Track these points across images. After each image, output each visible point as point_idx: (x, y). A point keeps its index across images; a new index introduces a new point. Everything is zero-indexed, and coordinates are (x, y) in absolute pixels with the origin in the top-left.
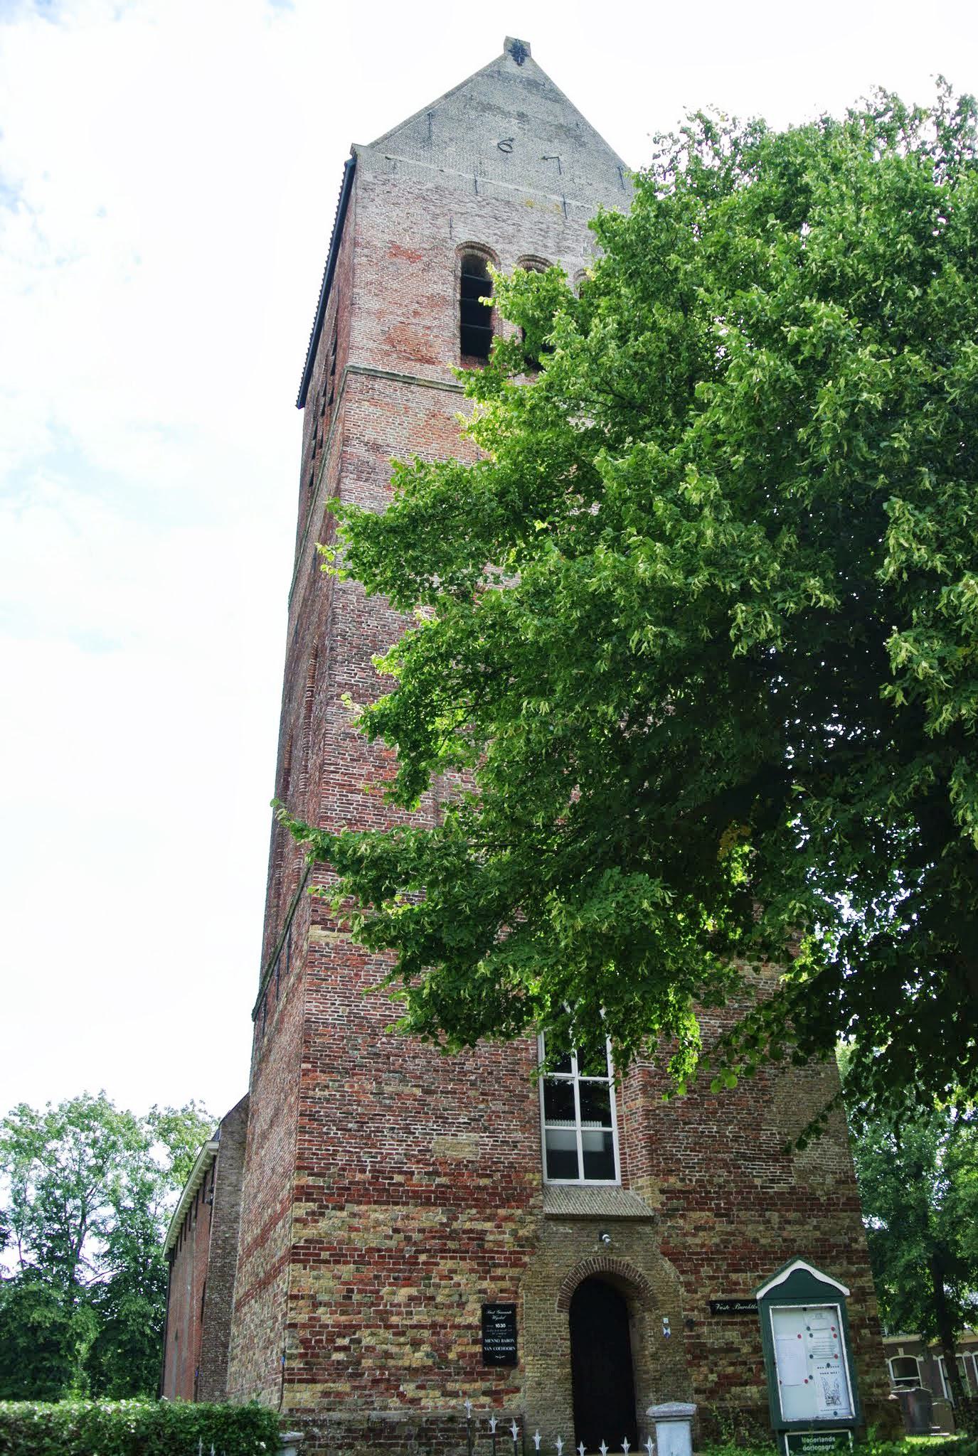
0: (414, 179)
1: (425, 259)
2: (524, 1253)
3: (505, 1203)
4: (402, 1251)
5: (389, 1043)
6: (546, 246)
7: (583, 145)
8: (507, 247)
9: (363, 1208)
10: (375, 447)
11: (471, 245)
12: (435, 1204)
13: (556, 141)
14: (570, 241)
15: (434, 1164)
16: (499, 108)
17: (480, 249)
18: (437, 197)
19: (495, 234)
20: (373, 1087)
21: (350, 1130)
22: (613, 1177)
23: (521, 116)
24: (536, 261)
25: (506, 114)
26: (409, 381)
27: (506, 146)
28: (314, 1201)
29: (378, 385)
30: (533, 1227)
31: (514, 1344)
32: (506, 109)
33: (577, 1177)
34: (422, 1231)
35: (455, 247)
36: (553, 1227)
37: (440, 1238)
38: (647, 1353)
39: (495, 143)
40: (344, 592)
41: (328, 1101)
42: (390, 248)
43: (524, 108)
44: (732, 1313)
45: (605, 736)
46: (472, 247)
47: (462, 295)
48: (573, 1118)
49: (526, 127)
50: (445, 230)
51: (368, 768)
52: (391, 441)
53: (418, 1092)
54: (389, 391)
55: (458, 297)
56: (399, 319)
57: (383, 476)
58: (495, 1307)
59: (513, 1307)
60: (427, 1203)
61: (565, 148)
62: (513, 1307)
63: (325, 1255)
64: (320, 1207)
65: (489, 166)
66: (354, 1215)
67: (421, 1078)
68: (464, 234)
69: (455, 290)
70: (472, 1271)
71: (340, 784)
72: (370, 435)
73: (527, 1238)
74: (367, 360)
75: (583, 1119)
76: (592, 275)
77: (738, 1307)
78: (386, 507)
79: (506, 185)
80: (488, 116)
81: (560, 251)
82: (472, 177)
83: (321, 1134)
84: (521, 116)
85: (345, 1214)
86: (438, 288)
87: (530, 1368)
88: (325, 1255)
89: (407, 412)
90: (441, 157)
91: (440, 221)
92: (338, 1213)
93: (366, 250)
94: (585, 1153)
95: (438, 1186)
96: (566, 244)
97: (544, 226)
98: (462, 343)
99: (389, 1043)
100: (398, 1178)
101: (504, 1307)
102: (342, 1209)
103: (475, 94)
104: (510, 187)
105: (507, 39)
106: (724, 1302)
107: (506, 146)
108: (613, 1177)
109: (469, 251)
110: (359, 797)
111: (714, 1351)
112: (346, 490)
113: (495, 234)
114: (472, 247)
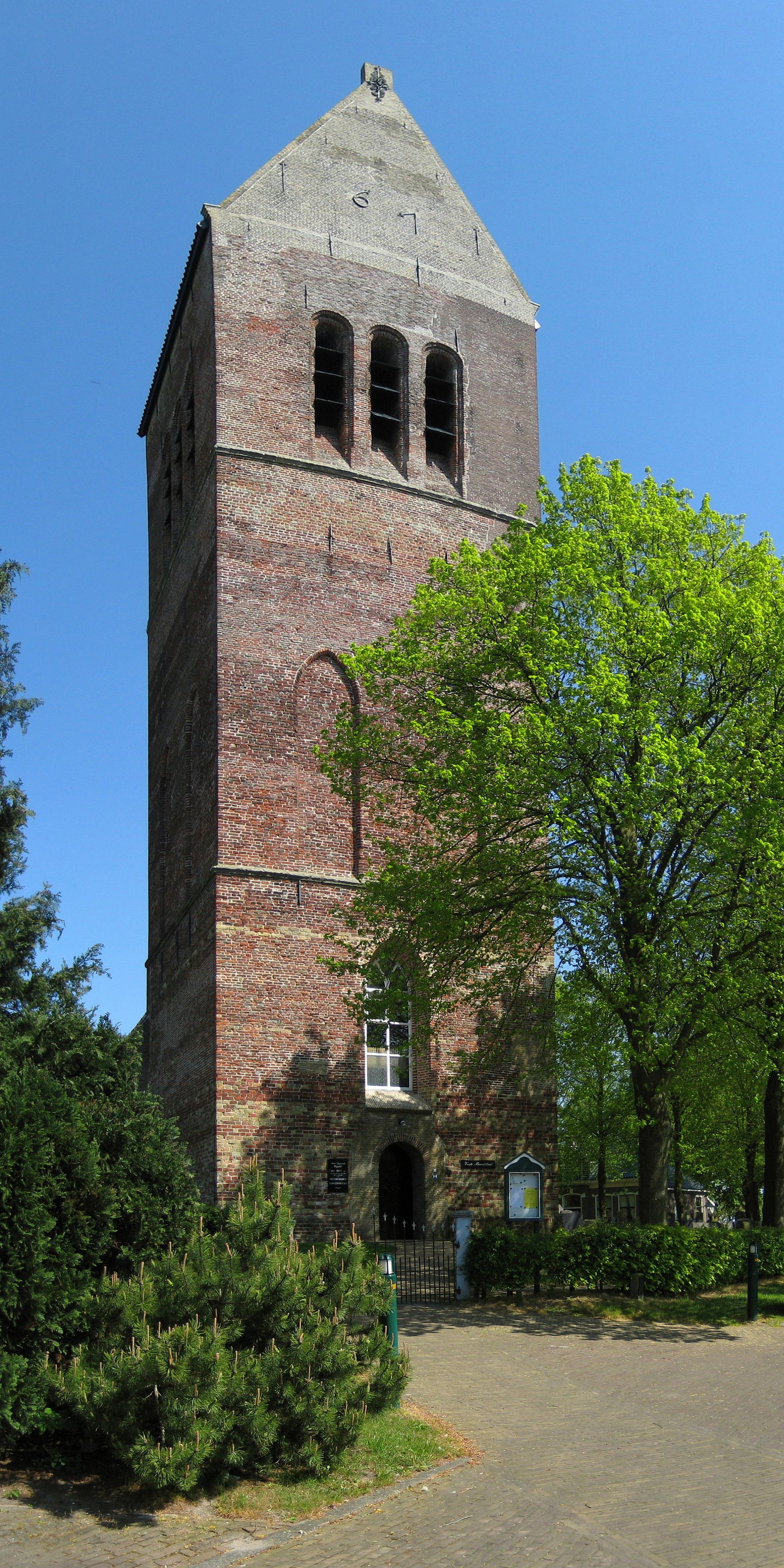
0: (268, 241)
1: (282, 331)
2: (353, 1130)
4: (281, 1128)
5: (270, 1000)
6: (397, 316)
7: (441, 200)
8: (360, 316)
9: (257, 1103)
10: (243, 526)
12: (300, 1101)
13: (413, 194)
14: (421, 312)
15: (299, 1077)
16: (355, 154)
18: (292, 261)
19: (350, 302)
20: (261, 1029)
21: (247, 1056)
22: (408, 1086)
23: (379, 163)
24: (387, 331)
25: (363, 161)
26: (269, 460)
27: (360, 202)
28: (228, 1099)
29: (243, 464)
30: (359, 1115)
31: (347, 1181)
32: (364, 154)
33: (386, 1085)
34: (292, 1116)
35: (309, 317)
36: (371, 1115)
37: (304, 1121)
38: (322, 1192)
39: (351, 195)
40: (225, 660)
41: (233, 1038)
42: (248, 320)
43: (380, 155)
47: (317, 367)
49: (384, 177)
50: (300, 299)
51: (249, 805)
52: (256, 518)
53: (289, 1032)
54: (253, 470)
55: (313, 369)
56: (259, 396)
57: (252, 553)
58: (335, 1160)
59: (346, 1161)
60: (296, 1100)
61: (423, 202)
63: (236, 1131)
64: (231, 1103)
65: (344, 224)
66: (252, 1107)
67: (291, 1023)
68: (318, 303)
69: (310, 363)
70: (322, 1140)
71: (230, 818)
72: (239, 513)
73: (355, 1122)
74: (231, 439)
77: (478, 1164)
78: (613, 534)
79: (360, 245)
80: (342, 165)
81: (411, 322)
82: (324, 236)
83: (230, 1059)
84: (379, 163)
85: (247, 1106)
86: (294, 362)
88: (236, 1131)
89: (269, 491)
90: (295, 215)
91: (296, 289)
92: (243, 1106)
93: (225, 324)
94: (368, 1069)
95: (302, 1090)
96: (418, 314)
97: (397, 294)
98: (316, 417)
99: (270, 1000)
102: (245, 1104)
103: (329, 137)
104: (365, 248)
107: (360, 202)
108: (408, 1086)
109: (324, 319)
110: (243, 827)
112: (222, 568)
113: (350, 302)
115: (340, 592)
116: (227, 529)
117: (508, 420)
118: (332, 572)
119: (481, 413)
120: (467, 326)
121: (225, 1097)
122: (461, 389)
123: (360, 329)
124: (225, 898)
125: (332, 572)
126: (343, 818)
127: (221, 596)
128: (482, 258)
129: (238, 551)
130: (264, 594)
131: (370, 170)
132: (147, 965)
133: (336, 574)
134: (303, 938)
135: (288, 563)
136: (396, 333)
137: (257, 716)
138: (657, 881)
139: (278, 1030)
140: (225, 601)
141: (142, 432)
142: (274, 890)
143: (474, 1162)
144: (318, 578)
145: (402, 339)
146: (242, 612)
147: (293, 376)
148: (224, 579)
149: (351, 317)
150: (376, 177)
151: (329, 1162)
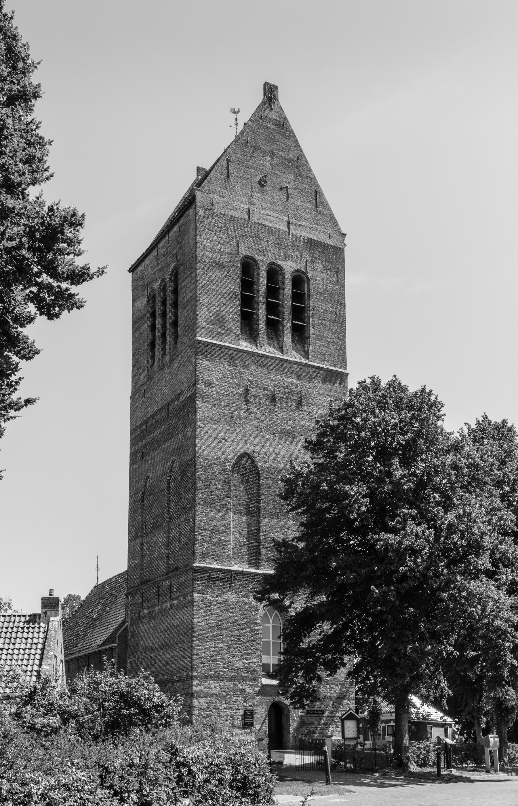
3: (251, 681)
6: (280, 256)
10: (208, 384)
11: (247, 257)
17: (251, 259)
19: (258, 249)
25: (265, 153)
39: (259, 177)
42: (212, 263)
44: (313, 713)
45: (373, 676)
46: (247, 258)
48: (273, 665)
59: (253, 710)
62: (253, 710)
68: (244, 251)
75: (270, 642)
76: (197, 385)
77: (315, 712)
81: (287, 257)
82: (246, 207)
87: (257, 726)
97: (279, 241)
100: (221, 673)
101: (250, 710)
102: (206, 682)
105: (266, 84)
106: (311, 711)
111: (307, 724)
114: (247, 258)
115: (252, 420)
116: (201, 386)
117: (331, 311)
118: (248, 409)
119: (318, 309)
120: (312, 256)
121: (197, 678)
122: (309, 296)
123: (262, 266)
124: (198, 580)
125: (248, 409)
126: (251, 538)
127: (198, 423)
128: (320, 209)
129: (206, 399)
130: (217, 422)
131: (268, 158)
132: (131, 398)
133: (250, 410)
134: (233, 600)
135: (228, 405)
136: (279, 266)
137: (213, 488)
138: (423, 466)
139: (222, 646)
140: (199, 426)
141: (133, 269)
142: (220, 576)
143: (314, 711)
144: (242, 413)
145: (282, 269)
146: (207, 432)
147: (231, 295)
148: (200, 415)
149: (259, 258)
150: (271, 164)
151: (245, 711)
